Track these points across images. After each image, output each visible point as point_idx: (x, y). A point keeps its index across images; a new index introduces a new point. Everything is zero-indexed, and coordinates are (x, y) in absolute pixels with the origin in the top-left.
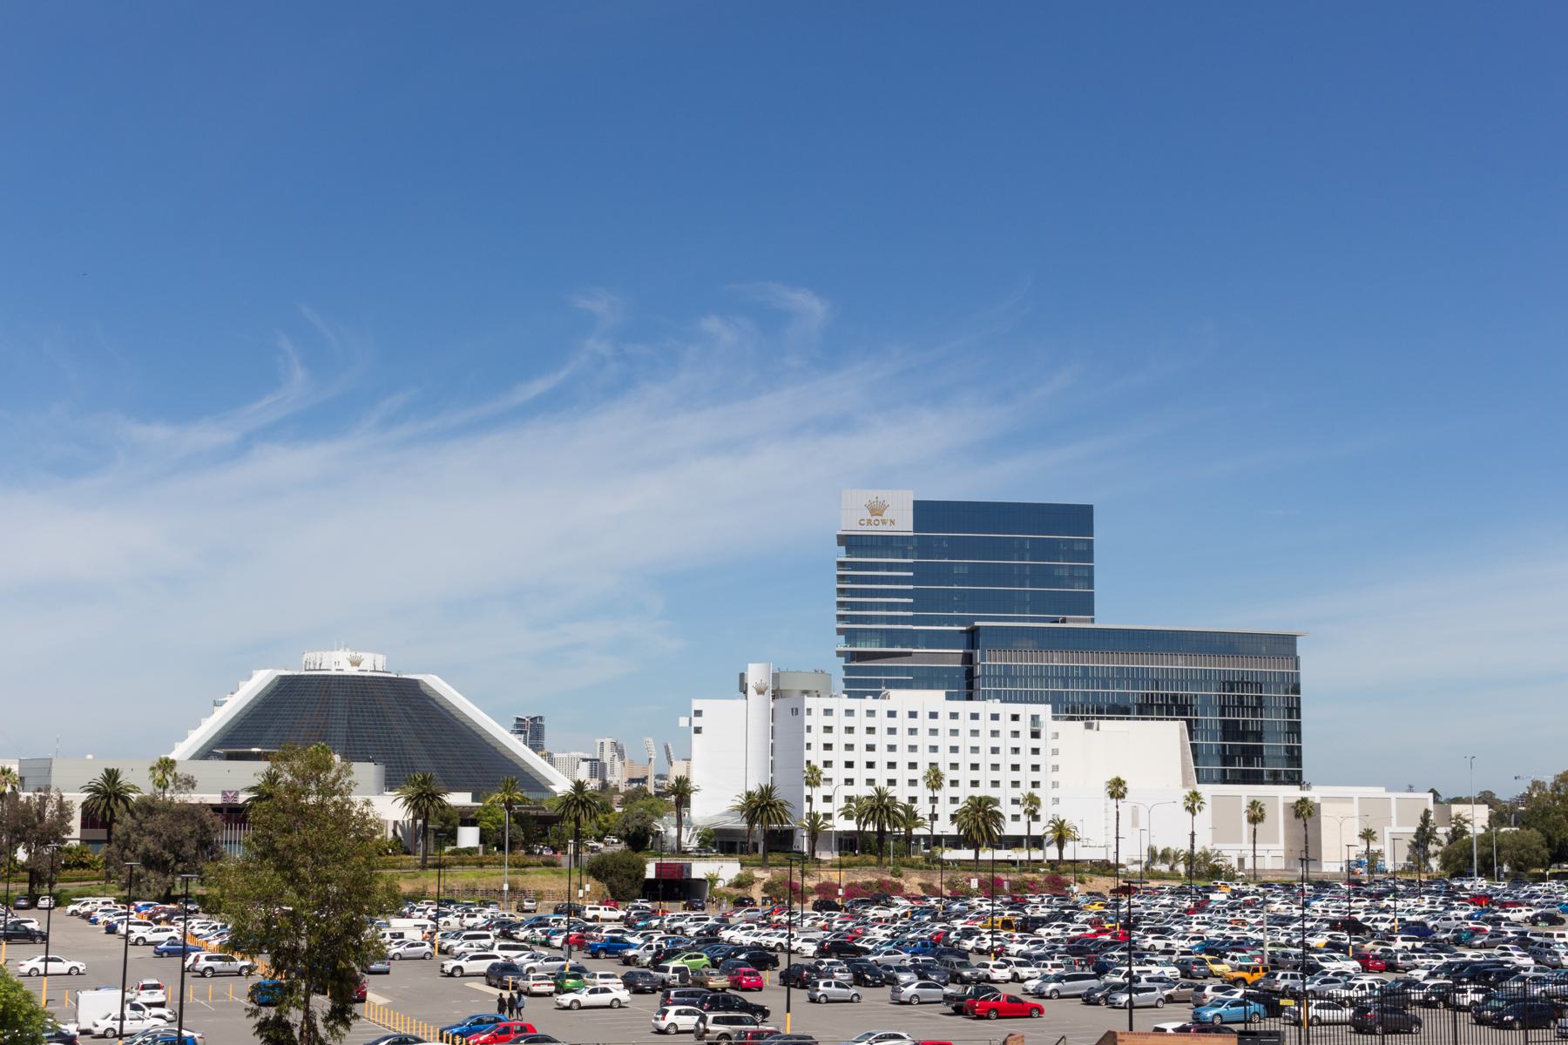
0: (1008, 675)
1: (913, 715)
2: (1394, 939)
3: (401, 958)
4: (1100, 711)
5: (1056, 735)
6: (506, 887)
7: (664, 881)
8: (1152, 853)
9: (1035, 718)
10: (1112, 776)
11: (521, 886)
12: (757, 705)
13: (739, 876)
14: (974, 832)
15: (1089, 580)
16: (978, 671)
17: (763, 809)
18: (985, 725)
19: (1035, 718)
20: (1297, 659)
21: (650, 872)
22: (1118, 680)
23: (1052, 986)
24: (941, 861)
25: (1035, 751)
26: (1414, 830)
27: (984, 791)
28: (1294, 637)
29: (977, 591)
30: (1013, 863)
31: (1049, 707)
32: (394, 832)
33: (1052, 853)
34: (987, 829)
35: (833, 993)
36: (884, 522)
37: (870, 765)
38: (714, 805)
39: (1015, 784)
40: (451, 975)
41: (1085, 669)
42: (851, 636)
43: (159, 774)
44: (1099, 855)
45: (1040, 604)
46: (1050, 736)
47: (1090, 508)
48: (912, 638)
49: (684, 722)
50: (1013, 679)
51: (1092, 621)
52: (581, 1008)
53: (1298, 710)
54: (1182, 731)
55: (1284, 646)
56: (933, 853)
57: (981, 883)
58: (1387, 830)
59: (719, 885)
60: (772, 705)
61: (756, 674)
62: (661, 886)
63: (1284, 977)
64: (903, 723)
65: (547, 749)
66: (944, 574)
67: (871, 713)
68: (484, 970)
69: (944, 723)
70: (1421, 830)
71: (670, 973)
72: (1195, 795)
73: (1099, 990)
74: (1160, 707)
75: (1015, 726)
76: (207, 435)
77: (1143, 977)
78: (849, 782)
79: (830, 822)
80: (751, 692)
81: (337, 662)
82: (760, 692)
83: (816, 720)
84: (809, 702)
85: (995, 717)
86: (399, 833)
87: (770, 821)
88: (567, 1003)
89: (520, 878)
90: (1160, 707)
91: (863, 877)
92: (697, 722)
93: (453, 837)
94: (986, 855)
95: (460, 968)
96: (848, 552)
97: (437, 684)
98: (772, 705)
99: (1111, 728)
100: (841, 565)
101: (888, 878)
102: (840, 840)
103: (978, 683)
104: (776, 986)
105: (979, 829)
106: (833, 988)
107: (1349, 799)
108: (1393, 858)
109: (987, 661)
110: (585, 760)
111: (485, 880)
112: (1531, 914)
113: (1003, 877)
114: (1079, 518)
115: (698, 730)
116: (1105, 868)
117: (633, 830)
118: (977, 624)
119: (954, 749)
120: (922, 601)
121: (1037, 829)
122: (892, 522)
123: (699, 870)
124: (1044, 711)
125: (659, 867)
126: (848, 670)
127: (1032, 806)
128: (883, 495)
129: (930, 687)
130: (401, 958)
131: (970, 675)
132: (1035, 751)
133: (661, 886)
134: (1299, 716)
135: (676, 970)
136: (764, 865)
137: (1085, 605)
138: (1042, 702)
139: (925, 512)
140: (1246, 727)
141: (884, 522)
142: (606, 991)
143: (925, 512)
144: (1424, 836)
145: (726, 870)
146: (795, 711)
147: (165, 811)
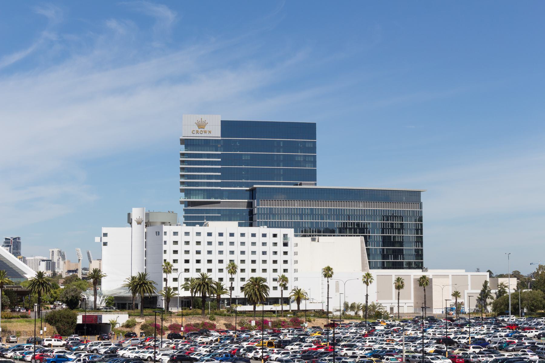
0: (271, 213)
1: (221, 235)
2: (469, 348)
4: (319, 232)
8: (346, 305)
9: (285, 236)
11: (8, 329)
12: (138, 230)
15: (314, 163)
16: (256, 211)
18: (259, 240)
19: (285, 236)
20: (421, 204)
21: (80, 320)
24: (236, 312)
25: (285, 253)
26: (479, 291)
30: (274, 312)
33: (294, 306)
34: (260, 294)
36: (205, 132)
38: (114, 283)
42: (188, 193)
44: (318, 307)
45: (288, 176)
46: (293, 245)
48: (221, 194)
49: (97, 239)
53: (421, 230)
54: (361, 241)
55: (414, 197)
58: (466, 292)
59: (117, 326)
61: (137, 213)
62: (85, 328)
64: (215, 239)
66: (238, 160)
70: (483, 291)
72: (368, 275)
75: (275, 240)
80: (134, 223)
82: (139, 223)
83: (169, 238)
84: (165, 228)
92: (105, 239)
96: (186, 148)
98: (145, 230)
99: (324, 240)
100: (182, 155)
101: (207, 321)
102: (182, 301)
109: (260, 206)
110: (43, 261)
114: (309, 130)
115: (105, 244)
116: (321, 314)
117: (70, 298)
118: (255, 186)
119: (187, 252)
120: (226, 174)
121: (286, 294)
122: (210, 132)
123: (106, 318)
124: (290, 232)
125: (84, 317)
126: (186, 211)
127: (284, 282)
128: (205, 117)
131: (251, 213)
134: (422, 233)
136: (141, 315)
137: (312, 176)
139: (226, 126)
140: (395, 240)
141: (205, 132)
143: (226, 126)
145: (121, 318)
146: (158, 233)
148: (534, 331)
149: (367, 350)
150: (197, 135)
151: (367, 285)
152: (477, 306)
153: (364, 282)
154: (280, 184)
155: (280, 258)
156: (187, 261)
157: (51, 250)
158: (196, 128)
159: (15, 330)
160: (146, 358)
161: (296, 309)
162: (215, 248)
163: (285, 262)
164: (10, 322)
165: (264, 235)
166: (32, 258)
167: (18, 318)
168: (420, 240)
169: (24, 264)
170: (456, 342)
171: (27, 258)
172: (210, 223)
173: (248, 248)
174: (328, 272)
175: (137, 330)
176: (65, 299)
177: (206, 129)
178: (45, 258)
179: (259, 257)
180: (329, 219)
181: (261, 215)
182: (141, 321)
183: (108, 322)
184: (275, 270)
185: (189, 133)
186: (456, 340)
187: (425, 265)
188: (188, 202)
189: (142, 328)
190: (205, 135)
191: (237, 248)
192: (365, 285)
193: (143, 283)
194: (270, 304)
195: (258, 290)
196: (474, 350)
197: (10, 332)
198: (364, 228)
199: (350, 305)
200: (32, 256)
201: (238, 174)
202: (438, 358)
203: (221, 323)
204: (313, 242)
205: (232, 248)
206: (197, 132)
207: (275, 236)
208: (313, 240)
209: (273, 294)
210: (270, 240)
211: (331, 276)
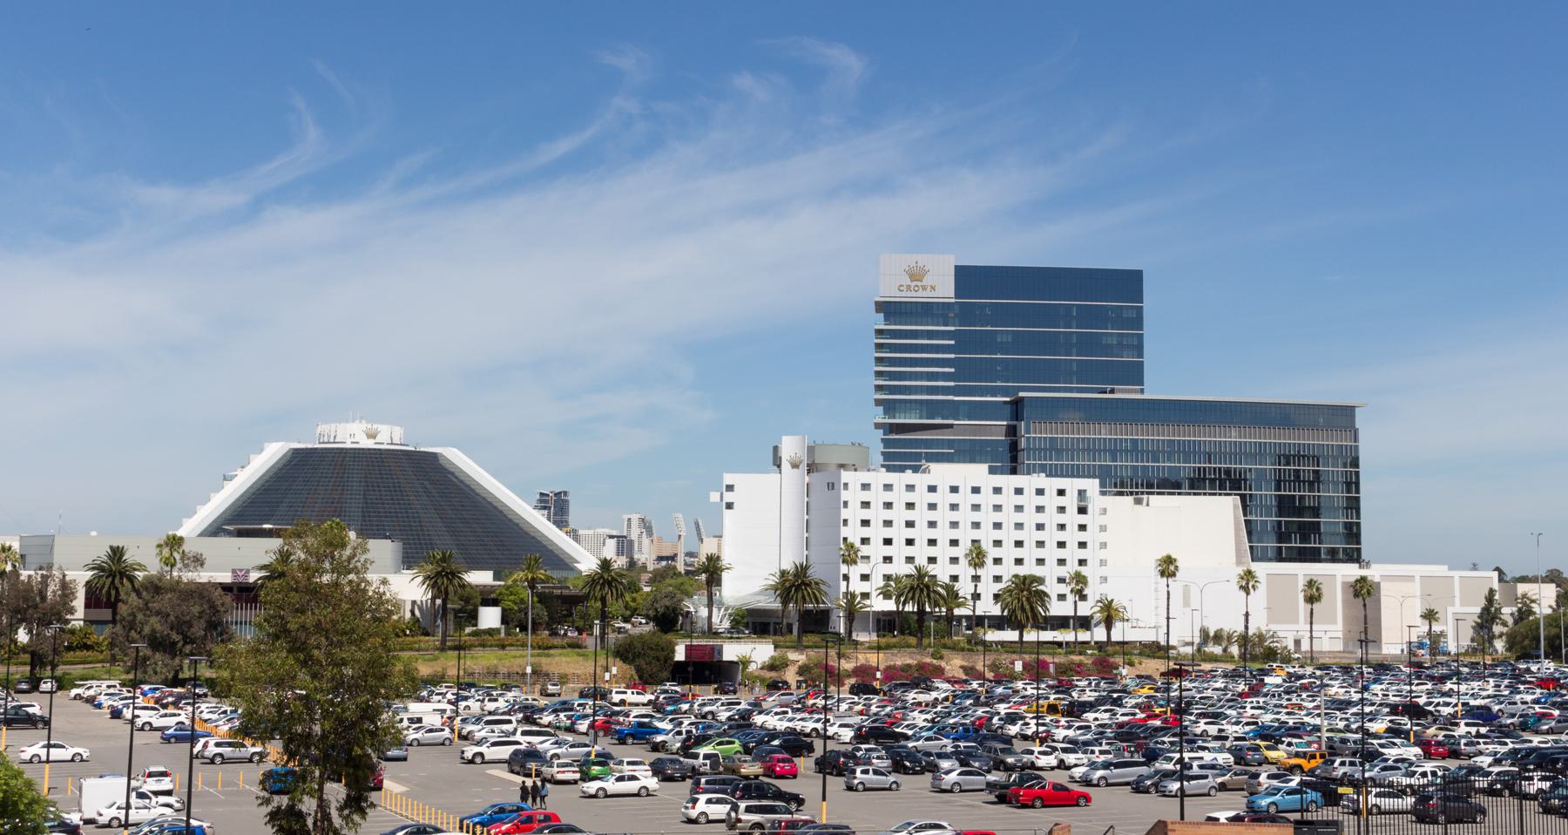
0: (1054, 448)
1: (954, 489)
2: (1457, 724)
4: (1150, 486)
5: (1104, 511)
6: (529, 670)
8: (1205, 634)
9: (1082, 494)
11: (545, 669)
12: (791, 480)
14: (1019, 613)
15: (1139, 349)
16: (1023, 444)
17: (798, 588)
20: (1356, 431)
21: (680, 655)
22: (1171, 453)
23: (1100, 773)
24: (984, 643)
26: (1478, 610)
29: (1022, 361)
30: (1060, 644)
32: (412, 612)
33: (1099, 634)
35: (871, 781)
36: (924, 288)
37: (910, 542)
38: (747, 582)
39: (1062, 562)
40: (471, 762)
41: (1135, 442)
42: (889, 407)
44: (1148, 636)
45: (1086, 374)
46: (1097, 511)
48: (954, 410)
49: (714, 497)
50: (1059, 452)
51: (1142, 391)
52: (607, 796)
54: (1235, 507)
55: (1342, 417)
57: (1025, 666)
58: (1450, 610)
59: (752, 667)
61: (791, 447)
62: (690, 669)
63: (1343, 764)
64: (943, 498)
66: (986, 342)
68: (507, 757)
70: (1486, 610)
71: (701, 760)
73: (1149, 778)
74: (1212, 481)
75: (1061, 501)
77: (1195, 764)
80: (785, 465)
81: (353, 435)
82: (795, 466)
83: (853, 496)
84: (846, 476)
85: (1040, 492)
86: (417, 613)
87: (804, 601)
88: (593, 791)
89: (544, 660)
91: (902, 659)
92: (728, 497)
93: (473, 617)
94: (1031, 636)
95: (481, 754)
96: (887, 319)
98: (807, 479)
99: (1161, 503)
100: (879, 332)
101: (928, 660)
102: (878, 621)
103: (1022, 456)
104: (811, 773)
105: (1023, 609)
106: (871, 776)
107: (1410, 578)
108: (1457, 640)
109: (1032, 433)
110: (611, 537)
113: (1049, 659)
114: (1129, 284)
115: (729, 506)
116: (1155, 650)
117: (661, 610)
118: (1021, 394)
119: (1040, 527)
120: (964, 370)
121: (1084, 609)
122: (933, 288)
124: (1092, 485)
125: (689, 649)
128: (923, 260)
129: (981, 462)
131: (1014, 448)
133: (690, 669)
134: (1358, 491)
135: (706, 757)
136: (799, 647)
137: (1135, 375)
139: (966, 277)
140: (1303, 504)
141: (924, 288)
142: (633, 778)
143: (966, 277)
144: (1488, 617)
145: (759, 652)
146: (831, 486)
149: (1248, 724)
152: (1473, 640)
154: (1071, 390)
155: (1072, 536)
157: (626, 517)
162: (943, 516)
165: (1040, 492)
173: (1008, 517)
174: (1167, 566)
176: (651, 613)
178: (614, 533)
179: (1030, 536)
185: (893, 289)
186: (1430, 708)
190: (925, 294)
191: (987, 517)
192: (1243, 594)
194: (1053, 629)
197: (547, 675)
207: (1061, 493)
208: (1138, 502)
210: (1051, 501)
211: (1174, 575)
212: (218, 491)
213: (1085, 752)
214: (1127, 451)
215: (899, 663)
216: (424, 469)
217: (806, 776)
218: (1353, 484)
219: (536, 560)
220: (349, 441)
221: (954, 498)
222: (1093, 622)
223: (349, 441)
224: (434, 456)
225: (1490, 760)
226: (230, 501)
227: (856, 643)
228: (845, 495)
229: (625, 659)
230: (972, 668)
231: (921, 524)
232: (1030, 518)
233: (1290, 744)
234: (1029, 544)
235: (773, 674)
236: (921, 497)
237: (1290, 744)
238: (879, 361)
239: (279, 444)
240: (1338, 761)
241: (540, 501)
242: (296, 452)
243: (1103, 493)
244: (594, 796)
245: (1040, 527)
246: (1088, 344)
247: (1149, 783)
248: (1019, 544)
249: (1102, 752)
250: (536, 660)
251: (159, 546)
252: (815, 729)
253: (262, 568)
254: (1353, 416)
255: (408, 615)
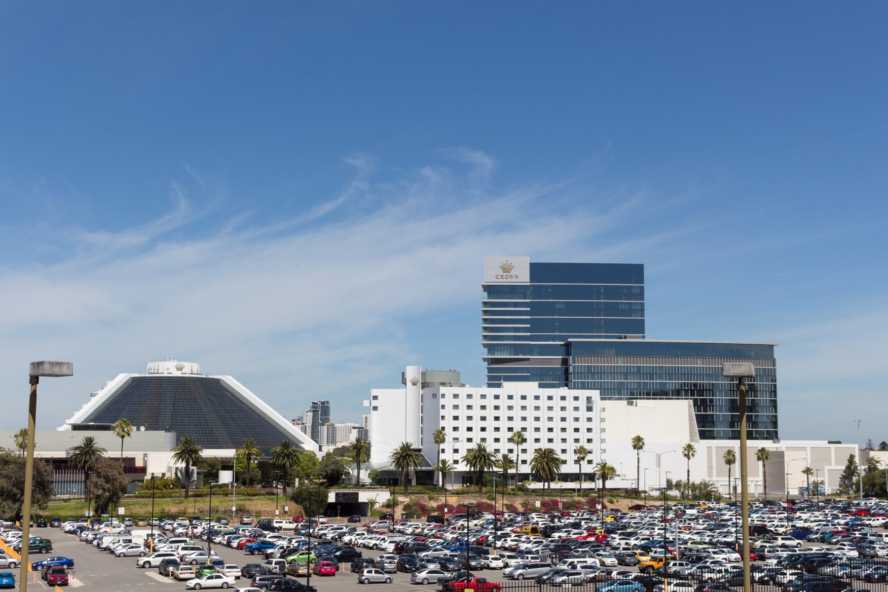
0: (590, 372)
1: (524, 397)
2: (776, 539)
3: (125, 556)
4: (648, 394)
5: (604, 410)
6: (234, 509)
7: (341, 504)
8: (669, 482)
9: (589, 399)
10: (635, 435)
11: (247, 508)
12: (412, 393)
13: (389, 500)
14: (541, 472)
15: (642, 311)
16: (571, 369)
17: (404, 458)
18: (557, 403)
19: (589, 399)
20: (774, 360)
21: (332, 498)
22: (650, 375)
23: (520, 571)
24: (527, 489)
25: (589, 420)
26: (844, 468)
27: (544, 445)
28: (772, 346)
29: (569, 322)
30: (574, 490)
31: (598, 392)
32: (176, 474)
33: (599, 484)
34: (549, 469)
35: (373, 578)
36: (511, 277)
37: (483, 429)
38: (381, 457)
39: (470, 440)
40: (143, 567)
41: (639, 367)
42: (491, 348)
43: (20, 439)
44: (629, 485)
45: (610, 327)
46: (599, 410)
47: (642, 265)
48: (530, 350)
49: (366, 403)
50: (593, 375)
51: (644, 337)
52: (201, 588)
53: (775, 392)
54: (689, 406)
55: (765, 352)
56: (523, 485)
57: (543, 504)
58: (827, 468)
59: (377, 506)
60: (421, 392)
61: (412, 373)
62: (339, 507)
63: (675, 565)
64: (517, 403)
65: (331, 422)
66: (550, 309)
67: (456, 396)
68: (158, 564)
69: (544, 403)
70: (848, 467)
71: (273, 565)
72: (689, 447)
73: (546, 574)
74: (686, 391)
75: (576, 404)
76: (132, 238)
77: (579, 566)
78: (537, 440)
79: (455, 466)
80: (409, 383)
81: (169, 369)
82: (414, 384)
83: (448, 401)
84: (443, 390)
85: (563, 398)
86: (179, 474)
87: (416, 465)
88: (192, 585)
89: (247, 503)
90: (686, 391)
91: (470, 500)
92: (375, 403)
93: (216, 477)
94: (554, 485)
95: (149, 562)
96: (489, 296)
97: (231, 382)
98: (421, 392)
99: (644, 405)
100: (485, 304)
101: (484, 501)
102: (463, 477)
103: (571, 377)
104: (349, 572)
105: (544, 470)
106: (373, 574)
107: (804, 449)
108: (830, 487)
109: (577, 363)
110: (354, 428)
111: (225, 504)
112: (884, 521)
113: (558, 499)
114: (635, 272)
115: (375, 408)
116: (634, 493)
117: (329, 472)
118: (570, 340)
119: (563, 419)
120: (536, 326)
121: (587, 469)
122: (517, 277)
123: (364, 497)
124: (595, 394)
125: (337, 495)
126: (490, 370)
127: (582, 454)
128: (512, 260)
129: (533, 381)
130: (125, 556)
131: (566, 372)
132: (589, 420)
133: (339, 507)
134: (775, 396)
135: (277, 563)
136: (405, 493)
137: (639, 327)
138: (595, 389)
139: (537, 270)
140: (736, 403)
141: (511, 277)
142: (220, 577)
143: (537, 270)
144: (850, 470)
145: (382, 496)
146: (435, 396)
147: (15, 463)
148: (880, 518)
149: (643, 539)
150: (502, 280)
151: (689, 459)
152: (840, 486)
153: (685, 455)
154: (600, 337)
155: (583, 425)
156: (470, 429)
157: (364, 416)
158: (501, 272)
159: (254, 509)
160: (371, 545)
161: (601, 487)
162: (503, 413)
163: (589, 430)
164: (250, 500)
165: (563, 398)
166: (343, 425)
167: (263, 495)
168: (774, 404)
169: (303, 434)
170: (771, 531)
171: (336, 425)
172: (506, 384)
173: (544, 414)
174: (646, 442)
175: (399, 512)
176: (324, 473)
177: (512, 273)
178: (357, 426)
179: (557, 425)
180: (660, 379)
181: (579, 374)
182: (403, 499)
183: (366, 501)
184: (470, 440)
185: (492, 280)
186: (772, 529)
187: (779, 436)
188: (492, 359)
189: (404, 509)
190: (512, 280)
191: (530, 414)
192: (686, 459)
193: (407, 455)
194: (572, 481)
195: (547, 463)
196: (784, 542)
197: (248, 511)
198: (703, 391)
199: (674, 483)
200: (342, 423)
201: (550, 326)
202: (723, 552)
203: (500, 503)
204: (630, 407)
205: (524, 414)
206: (502, 276)
207: (576, 398)
208: (631, 404)
209: (569, 468)
210: (570, 404)
211: (641, 448)
212: (86, 403)
213: (523, 558)
214: (634, 373)
215: (466, 503)
216: (211, 391)
217: (342, 574)
218: (774, 392)
219: (251, 443)
220: (166, 372)
221: (524, 403)
222: (597, 476)
223: (166, 372)
224: (218, 381)
225: (775, 561)
226: (91, 411)
227: (446, 490)
228: (442, 401)
229: (297, 502)
230: (511, 506)
231: (570, 420)
232: (557, 414)
233: (656, 552)
234: (557, 430)
235: (389, 510)
236: (503, 402)
237: (656, 552)
238: (485, 321)
239: (124, 375)
240: (672, 563)
241: (313, 407)
242: (134, 379)
243: (602, 399)
244: (193, 589)
245: (563, 419)
246: (610, 309)
247: (545, 577)
248: (577, 430)
249: (532, 558)
250: (240, 502)
251: (16, 436)
252: (376, 545)
253: (77, 448)
254: (772, 351)
255: (173, 476)
